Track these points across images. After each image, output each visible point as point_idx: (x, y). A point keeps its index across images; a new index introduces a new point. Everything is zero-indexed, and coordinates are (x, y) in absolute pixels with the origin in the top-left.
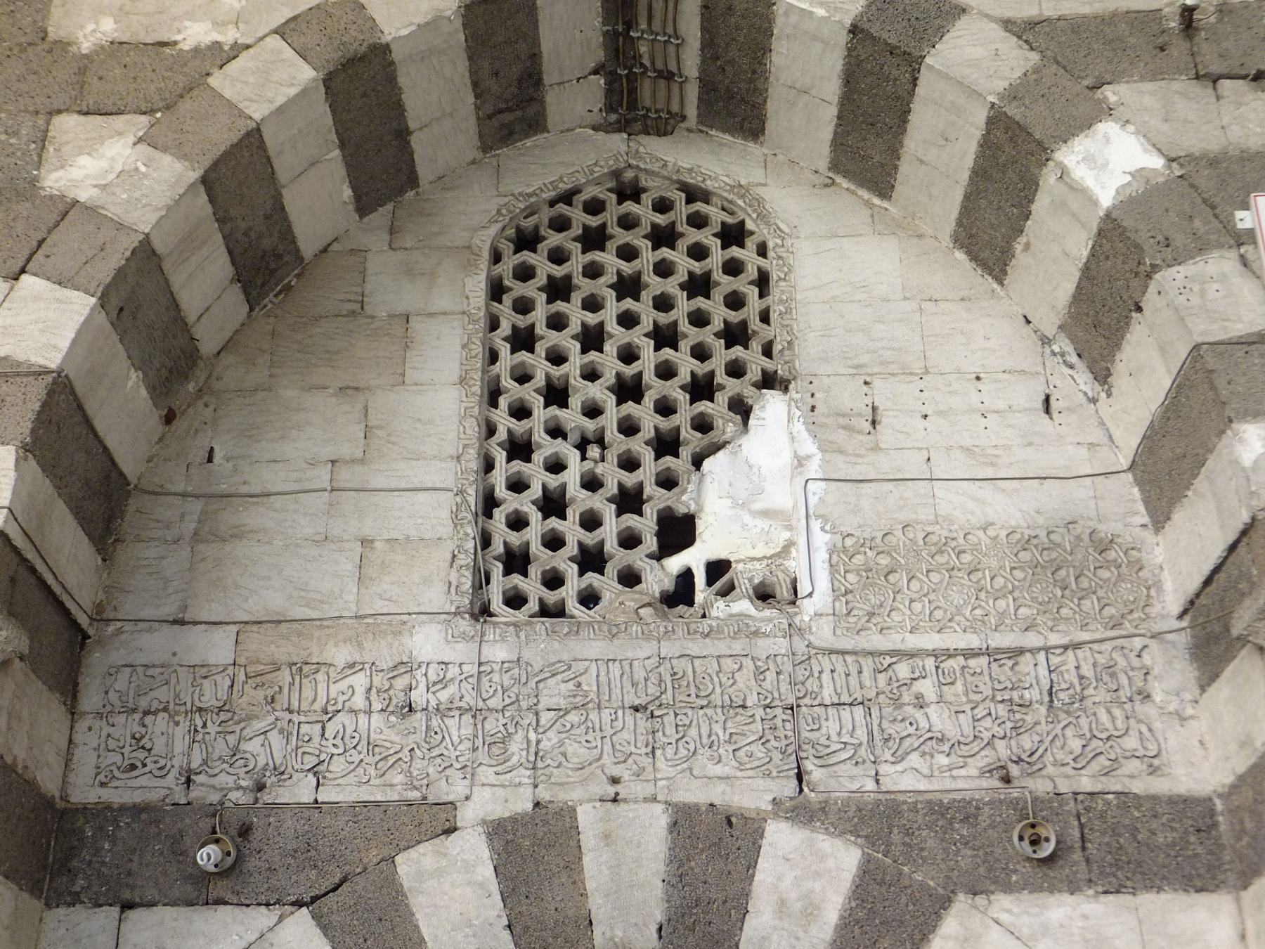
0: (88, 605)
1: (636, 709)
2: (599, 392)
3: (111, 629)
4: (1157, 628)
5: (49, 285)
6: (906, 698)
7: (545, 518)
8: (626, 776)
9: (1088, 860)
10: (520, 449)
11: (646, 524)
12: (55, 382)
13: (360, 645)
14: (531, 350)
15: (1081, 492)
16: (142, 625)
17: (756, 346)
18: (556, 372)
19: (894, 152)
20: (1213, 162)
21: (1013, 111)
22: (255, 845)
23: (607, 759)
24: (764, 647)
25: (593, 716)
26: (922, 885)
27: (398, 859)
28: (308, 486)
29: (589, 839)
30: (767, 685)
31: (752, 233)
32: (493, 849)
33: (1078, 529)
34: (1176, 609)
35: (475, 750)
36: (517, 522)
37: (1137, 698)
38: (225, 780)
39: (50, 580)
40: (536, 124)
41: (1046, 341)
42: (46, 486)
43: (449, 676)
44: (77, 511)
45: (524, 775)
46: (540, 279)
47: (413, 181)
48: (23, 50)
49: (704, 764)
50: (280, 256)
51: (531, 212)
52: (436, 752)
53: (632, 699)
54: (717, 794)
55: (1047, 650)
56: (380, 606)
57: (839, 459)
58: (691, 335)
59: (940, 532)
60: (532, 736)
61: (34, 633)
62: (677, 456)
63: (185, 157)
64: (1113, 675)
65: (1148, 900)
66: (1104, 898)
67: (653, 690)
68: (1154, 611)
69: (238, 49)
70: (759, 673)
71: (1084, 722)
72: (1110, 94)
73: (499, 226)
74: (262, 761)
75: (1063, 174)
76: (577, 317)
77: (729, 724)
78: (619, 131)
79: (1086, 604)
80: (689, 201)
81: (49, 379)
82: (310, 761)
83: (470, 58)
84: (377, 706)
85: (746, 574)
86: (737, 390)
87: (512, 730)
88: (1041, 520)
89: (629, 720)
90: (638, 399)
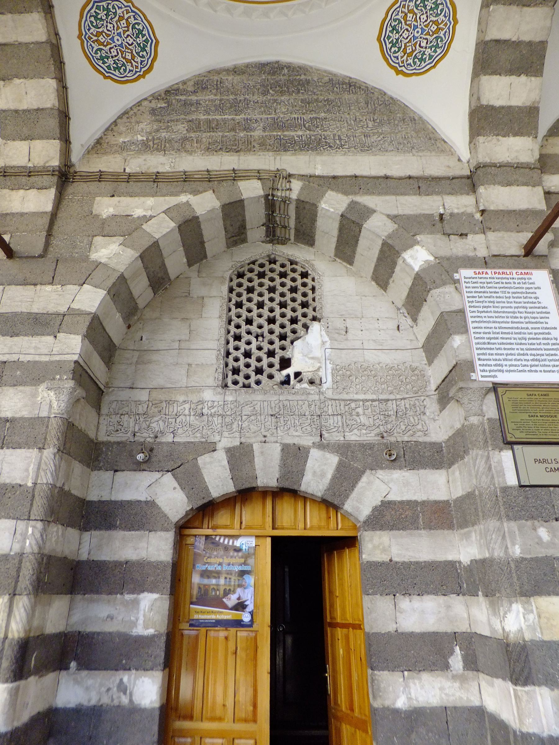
0: (104, 383)
1: (272, 415)
2: (262, 321)
3: (111, 390)
4: (429, 394)
5: (92, 287)
6: (354, 413)
7: (245, 358)
8: (268, 435)
9: (405, 461)
10: (238, 338)
11: (276, 361)
12: (93, 316)
13: (187, 396)
14: (241, 308)
15: (407, 354)
16: (120, 389)
17: (311, 308)
18: (249, 315)
19: (354, 252)
20: (448, 259)
21: (390, 242)
22: (155, 454)
23: (263, 430)
24: (311, 398)
25: (259, 417)
26: (357, 468)
27: (198, 459)
28: (171, 348)
29: (256, 453)
30: (312, 409)
31: (310, 274)
32: (227, 456)
33: (406, 365)
34: (434, 388)
35: (222, 427)
36: (236, 360)
37: (422, 414)
38: (145, 435)
39: (92, 375)
40: (244, 240)
41: (399, 309)
42: (91, 348)
43: (215, 405)
44: (100, 355)
45: (237, 434)
46: (245, 287)
47: (205, 257)
48: (85, 217)
49: (292, 432)
50: (164, 279)
51: (242, 267)
52: (210, 427)
53: (271, 412)
54: (296, 441)
55: (396, 400)
56: (193, 384)
57: (336, 343)
58: (291, 304)
59: (365, 365)
60: (240, 423)
61: (87, 391)
62: (274, 357)
63: (135, 249)
64: (415, 407)
65: (422, 472)
66: (409, 471)
67: (277, 410)
68: (428, 389)
69: (151, 217)
70: (310, 406)
71: (406, 421)
72: (418, 238)
73: (232, 271)
74: (157, 429)
75: (404, 260)
76: (256, 298)
77: (300, 420)
78: (270, 243)
79: (408, 387)
80: (291, 264)
81: (92, 315)
82: (172, 430)
83: (224, 221)
84: (192, 414)
85: (306, 376)
86: (305, 321)
87: (233, 421)
88: (395, 362)
89: (270, 419)
90: (274, 323)
